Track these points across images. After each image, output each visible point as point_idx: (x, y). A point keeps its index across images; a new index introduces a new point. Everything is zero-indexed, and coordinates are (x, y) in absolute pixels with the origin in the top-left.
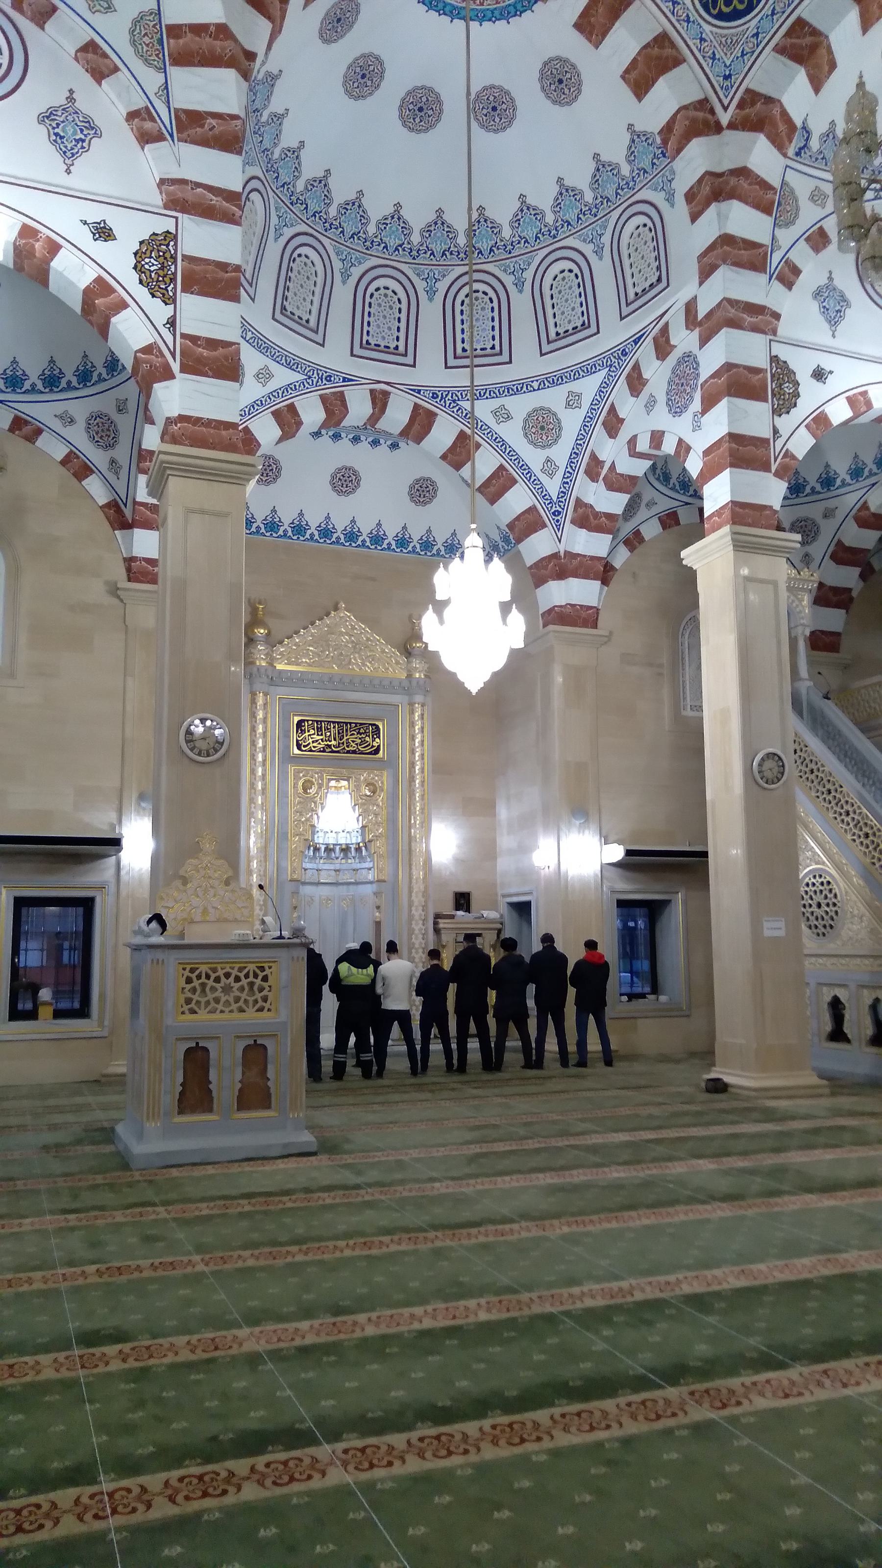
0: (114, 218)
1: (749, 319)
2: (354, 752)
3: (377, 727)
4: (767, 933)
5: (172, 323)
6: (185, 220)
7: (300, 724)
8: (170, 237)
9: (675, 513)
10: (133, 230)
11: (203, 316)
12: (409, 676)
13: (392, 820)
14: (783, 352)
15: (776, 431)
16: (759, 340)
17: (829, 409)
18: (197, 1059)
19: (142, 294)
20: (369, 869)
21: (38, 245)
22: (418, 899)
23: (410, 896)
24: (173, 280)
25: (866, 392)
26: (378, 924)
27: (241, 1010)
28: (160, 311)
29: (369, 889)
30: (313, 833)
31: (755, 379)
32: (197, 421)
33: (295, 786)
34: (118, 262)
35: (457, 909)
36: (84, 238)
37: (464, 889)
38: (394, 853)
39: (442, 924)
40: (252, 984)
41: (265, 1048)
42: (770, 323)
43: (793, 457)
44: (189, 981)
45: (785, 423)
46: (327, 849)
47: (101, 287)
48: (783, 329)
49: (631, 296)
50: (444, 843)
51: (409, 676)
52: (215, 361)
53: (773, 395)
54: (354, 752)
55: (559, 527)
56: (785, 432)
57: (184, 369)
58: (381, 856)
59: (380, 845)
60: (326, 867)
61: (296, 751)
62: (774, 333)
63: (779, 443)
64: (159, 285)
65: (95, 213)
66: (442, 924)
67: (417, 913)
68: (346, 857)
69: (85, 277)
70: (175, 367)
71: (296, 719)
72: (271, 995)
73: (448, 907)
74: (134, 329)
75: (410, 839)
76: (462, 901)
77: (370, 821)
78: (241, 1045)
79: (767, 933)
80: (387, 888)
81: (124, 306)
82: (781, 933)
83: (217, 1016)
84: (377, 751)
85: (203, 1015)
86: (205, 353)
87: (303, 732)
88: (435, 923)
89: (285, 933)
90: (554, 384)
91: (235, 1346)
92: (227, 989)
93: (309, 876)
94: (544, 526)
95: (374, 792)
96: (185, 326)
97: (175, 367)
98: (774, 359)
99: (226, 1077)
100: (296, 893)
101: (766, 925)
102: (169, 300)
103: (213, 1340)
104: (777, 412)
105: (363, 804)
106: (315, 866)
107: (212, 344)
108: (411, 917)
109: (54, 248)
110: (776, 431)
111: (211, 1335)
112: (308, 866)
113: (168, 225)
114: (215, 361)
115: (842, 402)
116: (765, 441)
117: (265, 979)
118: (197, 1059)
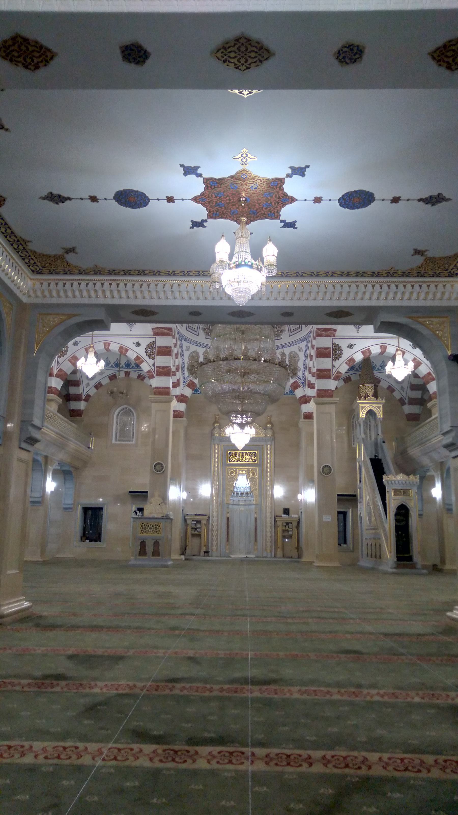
0: (140, 340)
1: (325, 333)
2: (248, 462)
3: (256, 453)
4: (324, 520)
5: (154, 364)
6: (158, 337)
7: (230, 453)
8: (154, 343)
9: (350, 377)
10: (145, 343)
11: (161, 361)
12: (266, 436)
13: (260, 484)
14: (336, 341)
15: (333, 366)
16: (329, 339)
17: (372, 349)
18: (143, 544)
19: (147, 358)
20: (252, 500)
21: (123, 351)
22: (269, 511)
23: (266, 509)
24: (155, 353)
25: (369, 349)
26: (256, 519)
27: (153, 533)
28: (151, 361)
29: (253, 507)
30: (234, 488)
31: (327, 351)
32: (160, 388)
33: (228, 473)
34: (141, 351)
35: (284, 514)
36: (133, 347)
37: (287, 507)
38: (260, 495)
39: (278, 519)
40: (156, 527)
41: (158, 542)
42: (333, 333)
43: (340, 373)
44: (142, 526)
45: (337, 363)
46: (241, 494)
47: (138, 358)
48: (337, 334)
49: (292, 330)
50: (279, 491)
51: (266, 436)
52: (165, 372)
53: (333, 355)
54: (248, 462)
55: (304, 387)
56: (337, 366)
57: (157, 375)
58: (256, 496)
59: (256, 492)
60: (241, 499)
61: (228, 462)
62: (334, 336)
63: (335, 370)
64: (151, 355)
65: (136, 340)
66: (278, 519)
67: (268, 515)
68: (242, 496)
69: (135, 355)
70: (155, 375)
71: (229, 452)
72: (161, 530)
73: (281, 513)
74: (145, 367)
75: (266, 490)
76: (286, 511)
77: (253, 484)
78: (153, 541)
79: (324, 520)
80: (259, 506)
81: (143, 361)
82: (330, 520)
83: (148, 534)
84: (255, 461)
85: (145, 534)
86: (162, 370)
87: (231, 456)
88: (275, 519)
89: (164, 516)
90: (294, 344)
91: (364, 767)
92: (150, 528)
93: (231, 502)
94: (300, 387)
95: (254, 475)
96: (157, 365)
97: (155, 375)
98: (334, 344)
99: (150, 548)
100: (228, 508)
101: (324, 517)
102: (153, 358)
103: (345, 758)
104: (334, 360)
105: (251, 480)
106: (237, 499)
107: (164, 368)
108: (266, 516)
109: (127, 350)
110: (333, 366)
111: (344, 754)
112: (231, 498)
113: (153, 339)
114: (165, 372)
115: (360, 353)
116: (329, 370)
117: (159, 526)
118: (143, 544)
